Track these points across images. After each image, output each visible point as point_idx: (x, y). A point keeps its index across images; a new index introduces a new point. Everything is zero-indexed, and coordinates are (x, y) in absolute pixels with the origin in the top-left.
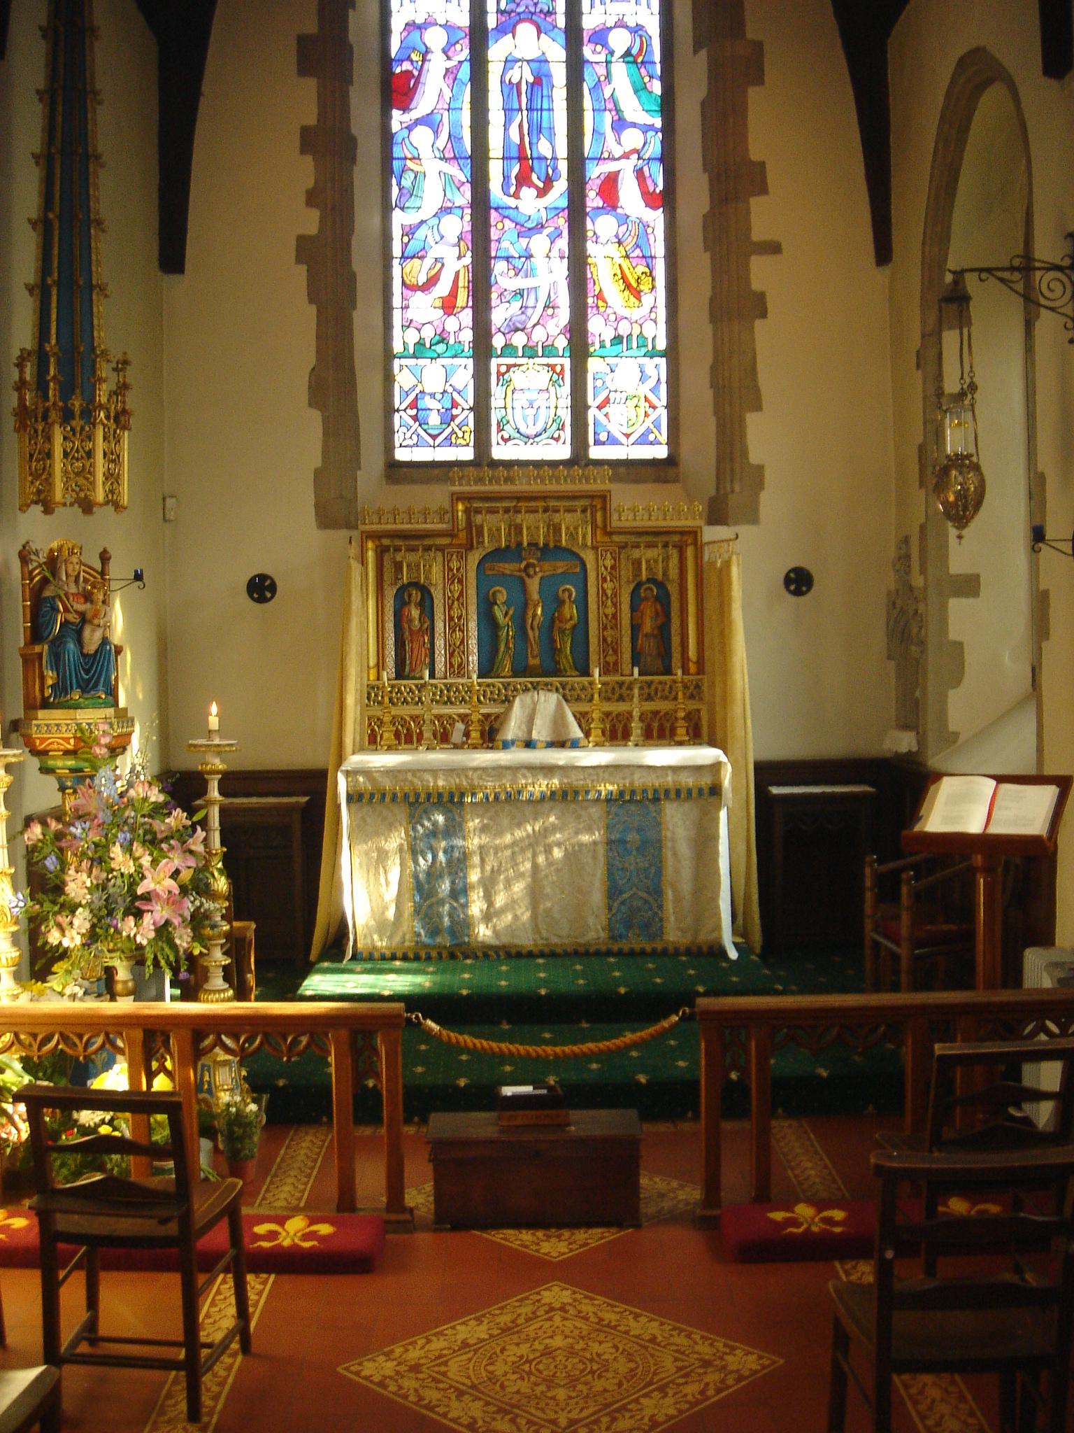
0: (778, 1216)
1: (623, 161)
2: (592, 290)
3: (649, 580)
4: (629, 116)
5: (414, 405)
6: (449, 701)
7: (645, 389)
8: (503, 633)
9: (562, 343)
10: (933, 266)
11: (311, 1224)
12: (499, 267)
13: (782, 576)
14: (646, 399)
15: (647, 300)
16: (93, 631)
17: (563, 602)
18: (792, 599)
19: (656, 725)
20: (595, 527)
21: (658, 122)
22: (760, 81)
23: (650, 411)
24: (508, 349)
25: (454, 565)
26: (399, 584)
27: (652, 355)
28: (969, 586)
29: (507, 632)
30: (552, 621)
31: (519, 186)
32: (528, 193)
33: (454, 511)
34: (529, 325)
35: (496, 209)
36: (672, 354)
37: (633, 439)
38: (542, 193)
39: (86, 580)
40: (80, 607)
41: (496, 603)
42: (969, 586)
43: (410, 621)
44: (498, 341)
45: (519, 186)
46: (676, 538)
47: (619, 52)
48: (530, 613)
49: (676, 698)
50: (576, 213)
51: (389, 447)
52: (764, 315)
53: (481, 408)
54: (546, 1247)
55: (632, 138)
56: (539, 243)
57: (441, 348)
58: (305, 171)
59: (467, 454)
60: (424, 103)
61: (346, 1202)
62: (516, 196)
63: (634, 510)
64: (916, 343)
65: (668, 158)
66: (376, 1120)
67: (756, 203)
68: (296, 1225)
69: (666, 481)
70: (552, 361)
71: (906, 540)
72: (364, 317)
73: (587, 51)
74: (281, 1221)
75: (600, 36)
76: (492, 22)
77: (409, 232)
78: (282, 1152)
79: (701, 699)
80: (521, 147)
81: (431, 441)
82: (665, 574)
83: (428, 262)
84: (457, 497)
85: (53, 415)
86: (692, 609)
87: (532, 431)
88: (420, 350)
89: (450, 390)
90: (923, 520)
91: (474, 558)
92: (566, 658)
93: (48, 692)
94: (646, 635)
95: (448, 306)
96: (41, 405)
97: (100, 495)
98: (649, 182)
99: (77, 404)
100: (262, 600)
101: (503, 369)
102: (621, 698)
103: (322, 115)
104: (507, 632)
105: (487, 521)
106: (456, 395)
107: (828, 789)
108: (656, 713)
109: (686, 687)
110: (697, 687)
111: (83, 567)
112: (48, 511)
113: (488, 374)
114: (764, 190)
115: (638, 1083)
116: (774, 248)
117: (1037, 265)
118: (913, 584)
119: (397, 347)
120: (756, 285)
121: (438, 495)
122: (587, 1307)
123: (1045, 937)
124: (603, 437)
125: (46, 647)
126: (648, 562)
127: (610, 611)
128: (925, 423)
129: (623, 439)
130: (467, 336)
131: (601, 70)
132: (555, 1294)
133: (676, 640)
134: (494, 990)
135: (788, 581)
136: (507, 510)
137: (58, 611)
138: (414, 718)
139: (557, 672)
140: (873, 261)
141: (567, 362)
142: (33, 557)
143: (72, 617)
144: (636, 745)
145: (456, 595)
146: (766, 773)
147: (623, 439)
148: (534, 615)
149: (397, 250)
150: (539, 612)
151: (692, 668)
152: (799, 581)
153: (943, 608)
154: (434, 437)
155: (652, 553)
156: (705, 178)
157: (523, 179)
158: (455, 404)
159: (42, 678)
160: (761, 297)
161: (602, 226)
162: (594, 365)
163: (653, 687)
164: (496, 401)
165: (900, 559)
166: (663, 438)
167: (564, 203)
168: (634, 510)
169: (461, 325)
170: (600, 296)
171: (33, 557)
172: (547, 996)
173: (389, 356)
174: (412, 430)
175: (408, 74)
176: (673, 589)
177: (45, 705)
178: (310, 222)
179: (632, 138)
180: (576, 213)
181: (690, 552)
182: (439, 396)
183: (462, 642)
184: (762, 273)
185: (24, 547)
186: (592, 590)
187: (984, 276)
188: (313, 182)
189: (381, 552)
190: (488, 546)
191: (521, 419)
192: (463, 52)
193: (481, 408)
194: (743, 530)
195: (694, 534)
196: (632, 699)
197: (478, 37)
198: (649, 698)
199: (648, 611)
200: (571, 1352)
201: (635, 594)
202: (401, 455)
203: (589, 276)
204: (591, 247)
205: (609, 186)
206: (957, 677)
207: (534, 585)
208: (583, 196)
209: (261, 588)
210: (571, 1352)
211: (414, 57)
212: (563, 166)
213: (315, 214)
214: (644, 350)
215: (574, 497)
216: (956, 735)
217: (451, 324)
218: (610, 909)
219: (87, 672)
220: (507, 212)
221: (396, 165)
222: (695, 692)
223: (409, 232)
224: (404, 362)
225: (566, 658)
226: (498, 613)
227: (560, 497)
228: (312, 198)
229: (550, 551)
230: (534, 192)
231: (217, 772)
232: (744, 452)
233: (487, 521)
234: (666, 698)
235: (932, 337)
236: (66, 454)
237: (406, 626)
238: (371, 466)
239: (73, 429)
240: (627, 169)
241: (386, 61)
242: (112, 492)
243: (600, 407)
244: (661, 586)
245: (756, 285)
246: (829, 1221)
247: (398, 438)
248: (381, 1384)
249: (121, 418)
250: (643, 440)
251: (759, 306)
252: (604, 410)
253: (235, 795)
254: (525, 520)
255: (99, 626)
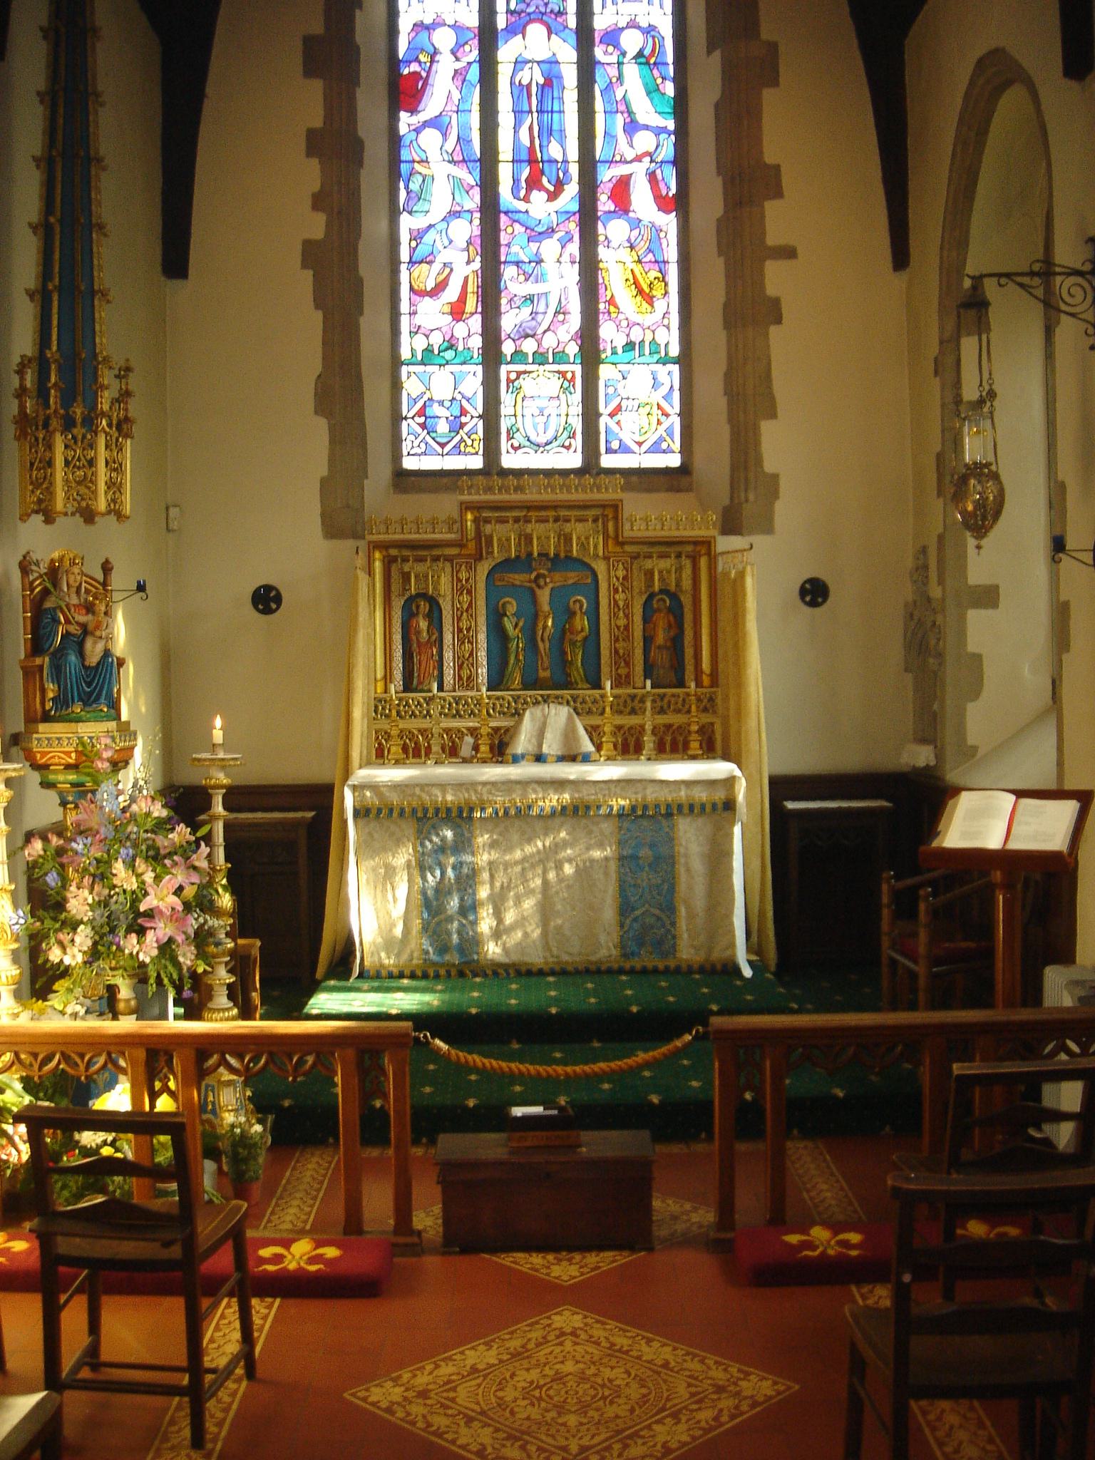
0: (793, 1239)
1: (636, 164)
2: (604, 296)
3: (661, 591)
4: (642, 118)
5: (422, 412)
6: (458, 715)
7: (657, 397)
8: (513, 645)
9: (573, 349)
10: (951, 271)
11: (317, 1247)
12: (509, 272)
13: (798, 587)
14: (659, 407)
15: (660, 305)
16: (95, 643)
17: (574, 613)
18: (808, 610)
19: (668, 739)
20: (606, 537)
21: (671, 125)
22: (775, 82)
23: (663, 419)
24: (518, 355)
25: (463, 575)
26: (407, 595)
27: (664, 361)
28: (988, 597)
29: (517, 644)
30: (563, 633)
31: (529, 190)
32: (538, 197)
33: (463, 521)
34: (540, 331)
35: (506, 213)
36: (685, 360)
37: (645, 447)
38: (552, 196)
39: (87, 591)
40: (82, 618)
41: (506, 615)
42: (988, 597)
43: (418, 632)
44: (508, 348)
45: (529, 190)
46: (689, 548)
47: (632, 53)
48: (540, 625)
49: (689, 712)
50: (588, 217)
51: (397, 456)
52: (779, 321)
53: (491, 415)
54: (556, 1271)
55: (645, 141)
56: (550, 248)
57: (449, 355)
58: (311, 175)
59: (476, 463)
60: (432, 105)
61: (353, 1224)
62: (526, 199)
63: (646, 520)
64: (934, 349)
65: (681, 161)
66: (384, 1141)
67: (771, 207)
68: (302, 1248)
69: (679, 491)
70: (563, 368)
71: (924, 550)
72: (371, 323)
73: (599, 52)
74: (287, 1244)
75: (612, 37)
76: (501, 22)
77: (417, 236)
78: (288, 1174)
79: (715, 712)
80: (531, 150)
81: (439, 449)
82: (678, 585)
83: (437, 267)
84: (466, 507)
85: (54, 423)
86: (705, 620)
87: (542, 439)
88: (428, 356)
89: (459, 397)
90: (941, 530)
91: (484, 568)
92: (577, 671)
93: (49, 705)
94: (659, 647)
95: (457, 311)
96: (41, 413)
97: (102, 505)
98: (662, 185)
99: (78, 412)
100: (267, 611)
101: (513, 376)
102: (633, 712)
103: (328, 117)
104: (517, 644)
105: (496, 531)
106: (464, 403)
107: (844, 804)
108: (668, 727)
109: (699, 700)
110: (711, 699)
111: (84, 578)
112: (49, 520)
113: (498, 381)
114: (779, 194)
115: (651, 1104)
116: (789, 253)
117: (1058, 270)
118: (931, 595)
119: (405, 354)
120: (771, 291)
121: (446, 505)
122: (598, 1332)
123: (1066, 955)
124: (615, 445)
125: (47, 659)
126: (660, 572)
127: (622, 622)
128: (943, 431)
129: (635, 447)
130: (476, 342)
131: (613, 72)
132: (566, 1319)
133: (689, 652)
134: (504, 1008)
135: (803, 592)
136: (517, 520)
137: (60, 622)
138: (422, 732)
139: (568, 685)
140: (890, 265)
141: (578, 369)
142: (34, 568)
143: (73, 629)
144: (649, 759)
145: (465, 606)
146: (781, 787)
147: (635, 447)
148: (545, 627)
149: (404, 255)
150: (550, 623)
151: (706, 680)
152: (814, 592)
153: (962, 619)
154: (443, 445)
155: (664, 564)
156: (719, 182)
157: (534, 183)
158: (463, 412)
159: (43, 691)
160: (776, 303)
161: (614, 231)
162: (605, 372)
163: (666, 700)
164: (506, 409)
165: (917, 569)
166: (676, 446)
167: (575, 207)
168: (646, 520)
169: (470, 331)
170: (611, 302)
171: (34, 568)
172: (557, 1014)
173: (396, 362)
174: (420, 438)
175: (416, 75)
176: (686, 600)
177: (46, 718)
178: (316, 227)
179: (645, 141)
180: (588, 217)
181: (703, 562)
182: (447, 404)
183: (471, 654)
184: (776, 279)
185: (24, 557)
186: (604, 602)
187: (1003, 281)
188: (319, 185)
189: (388, 563)
190: (498, 556)
191: (531, 427)
192: (472, 53)
193: (491, 415)
194: (758, 540)
195: (707, 544)
196: (644, 712)
197: (488, 37)
198: (662, 711)
199: (661, 622)
200: (582, 1378)
201: (647, 605)
202: (409, 463)
203: (601, 281)
204: (602, 252)
205: (621, 190)
206: (975, 690)
207: (544, 596)
208: (595, 200)
209: (266, 599)
210: (582, 1378)
211: (423, 58)
212: (574, 169)
213: (321, 219)
214: (656, 357)
215: (585, 507)
216: (975, 749)
217: (460, 330)
218: (622, 926)
219: (89, 685)
220: (516, 216)
221: (404, 168)
222: (708, 705)
223: (417, 236)
224: (412, 368)
225: (577, 671)
226: (508, 624)
227: (571, 506)
228: (318, 202)
229: (561, 562)
230: (544, 196)
231: (222, 787)
232: (759, 461)
233: (496, 531)
234: (679, 711)
235: (951, 344)
236: (67, 463)
237: (414, 638)
238: (379, 474)
239: (74, 438)
240: (639, 172)
241: (394, 62)
242: (114, 501)
243: (611, 415)
244: (674, 597)
245: (771, 291)
246: (845, 1244)
247: (406, 446)
248: (389, 1410)
249: (123, 426)
250: (656, 448)
251: (773, 312)
252: (616, 418)
253: (239, 810)
254: (535, 529)
255: (101, 637)
